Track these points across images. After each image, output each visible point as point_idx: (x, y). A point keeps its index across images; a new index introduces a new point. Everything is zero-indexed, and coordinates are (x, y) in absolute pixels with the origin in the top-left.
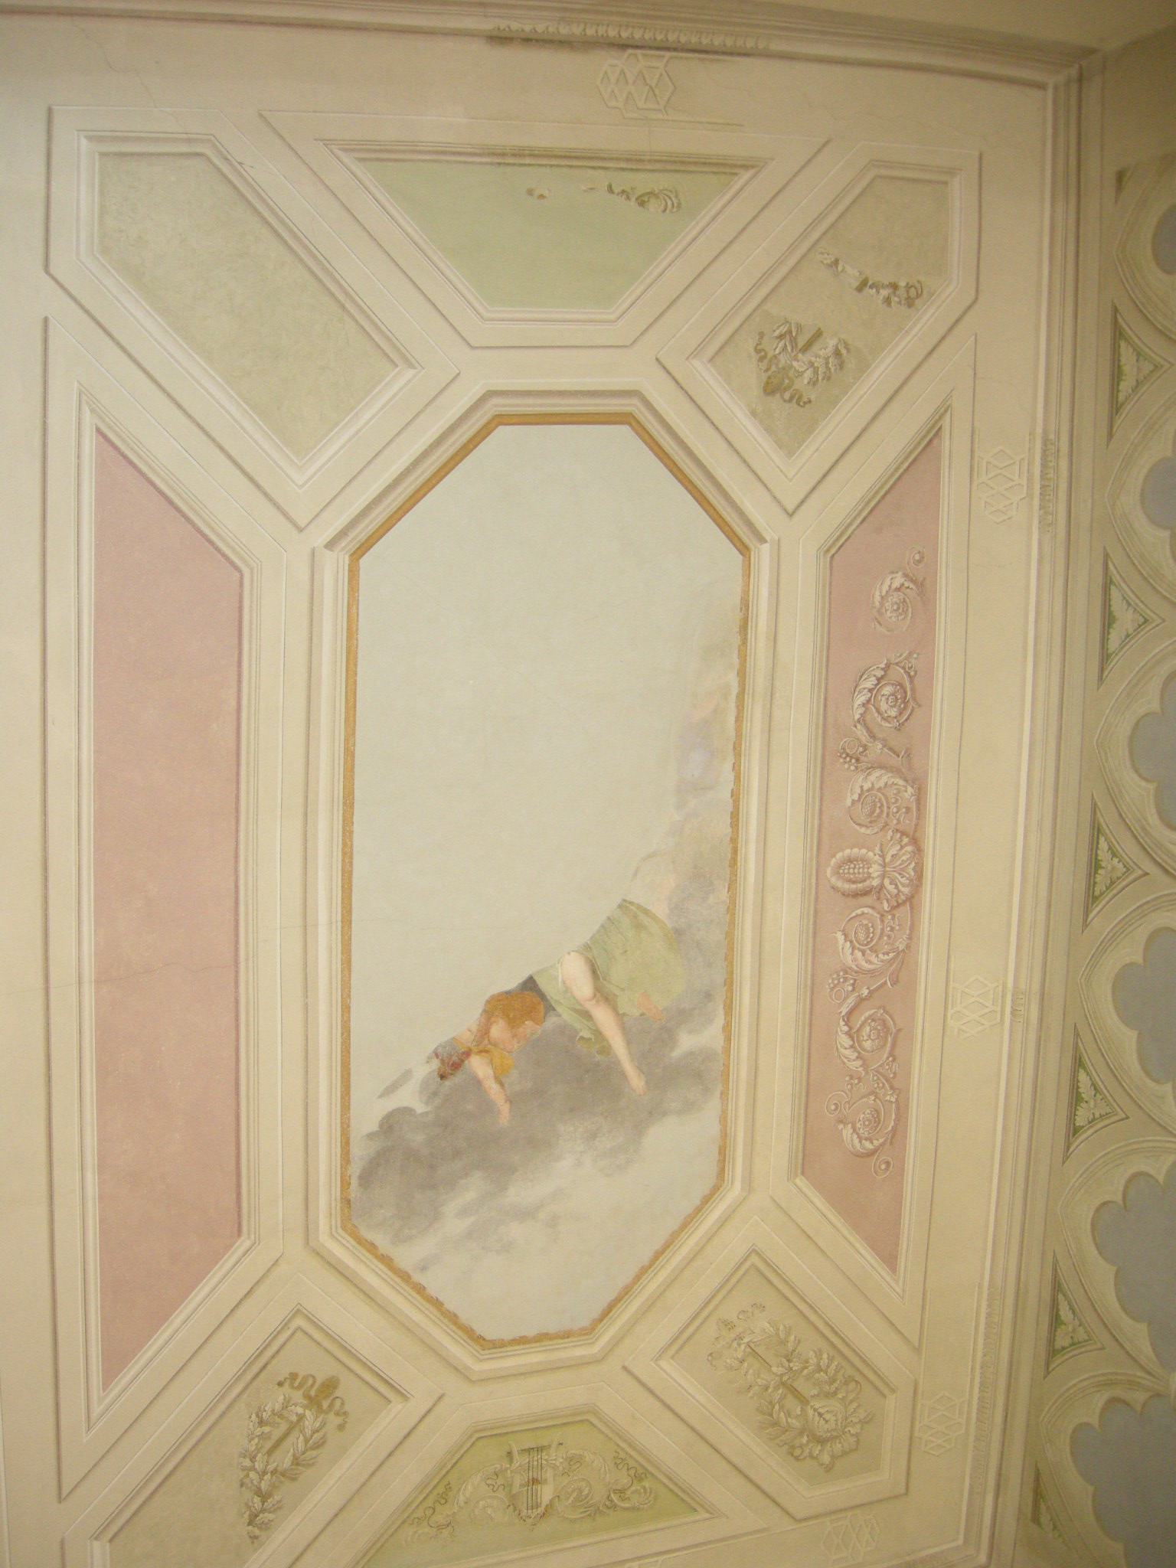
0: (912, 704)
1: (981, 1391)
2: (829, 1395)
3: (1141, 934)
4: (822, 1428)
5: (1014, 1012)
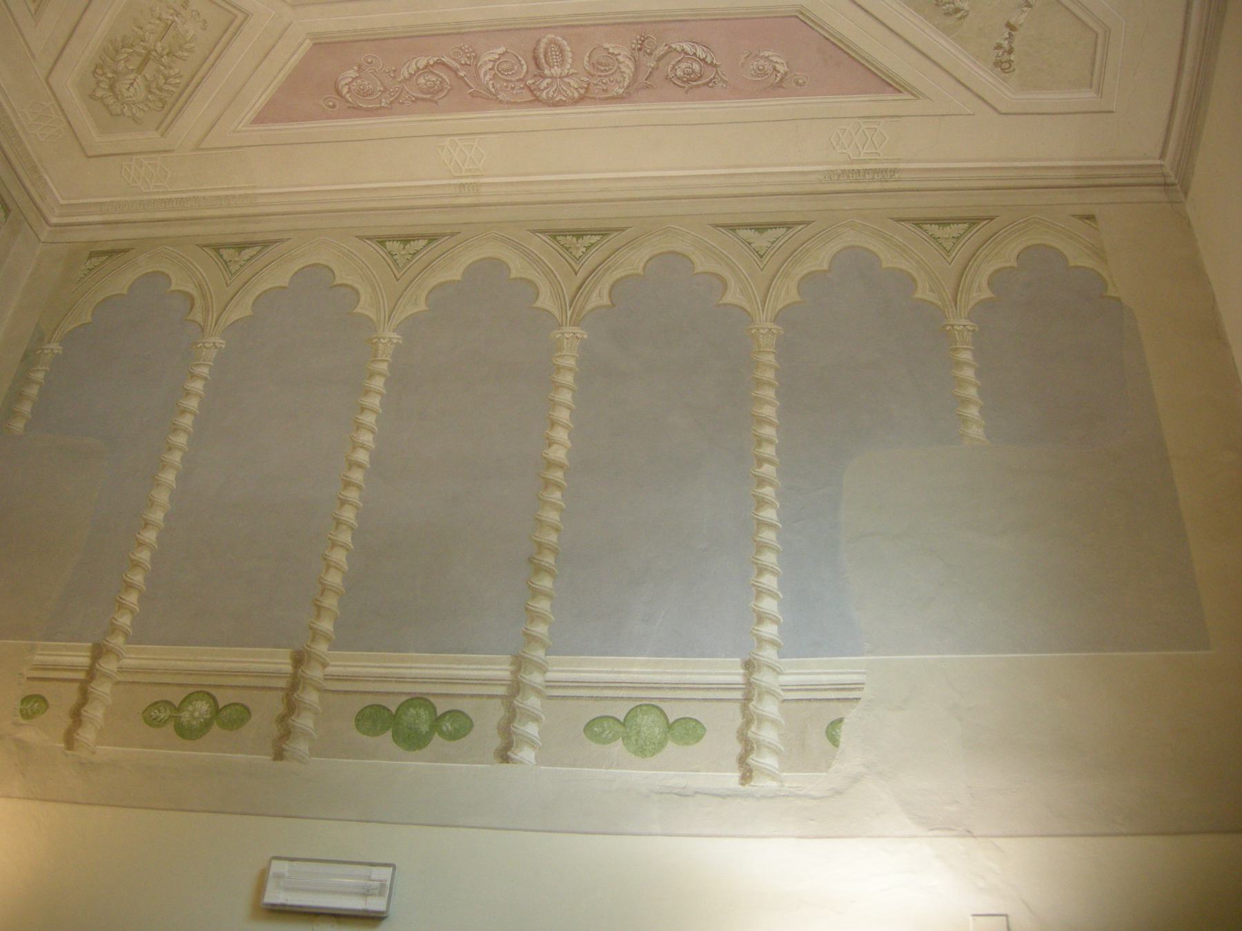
0: (687, 86)
1: (177, 199)
3: (532, 274)
5: (462, 185)
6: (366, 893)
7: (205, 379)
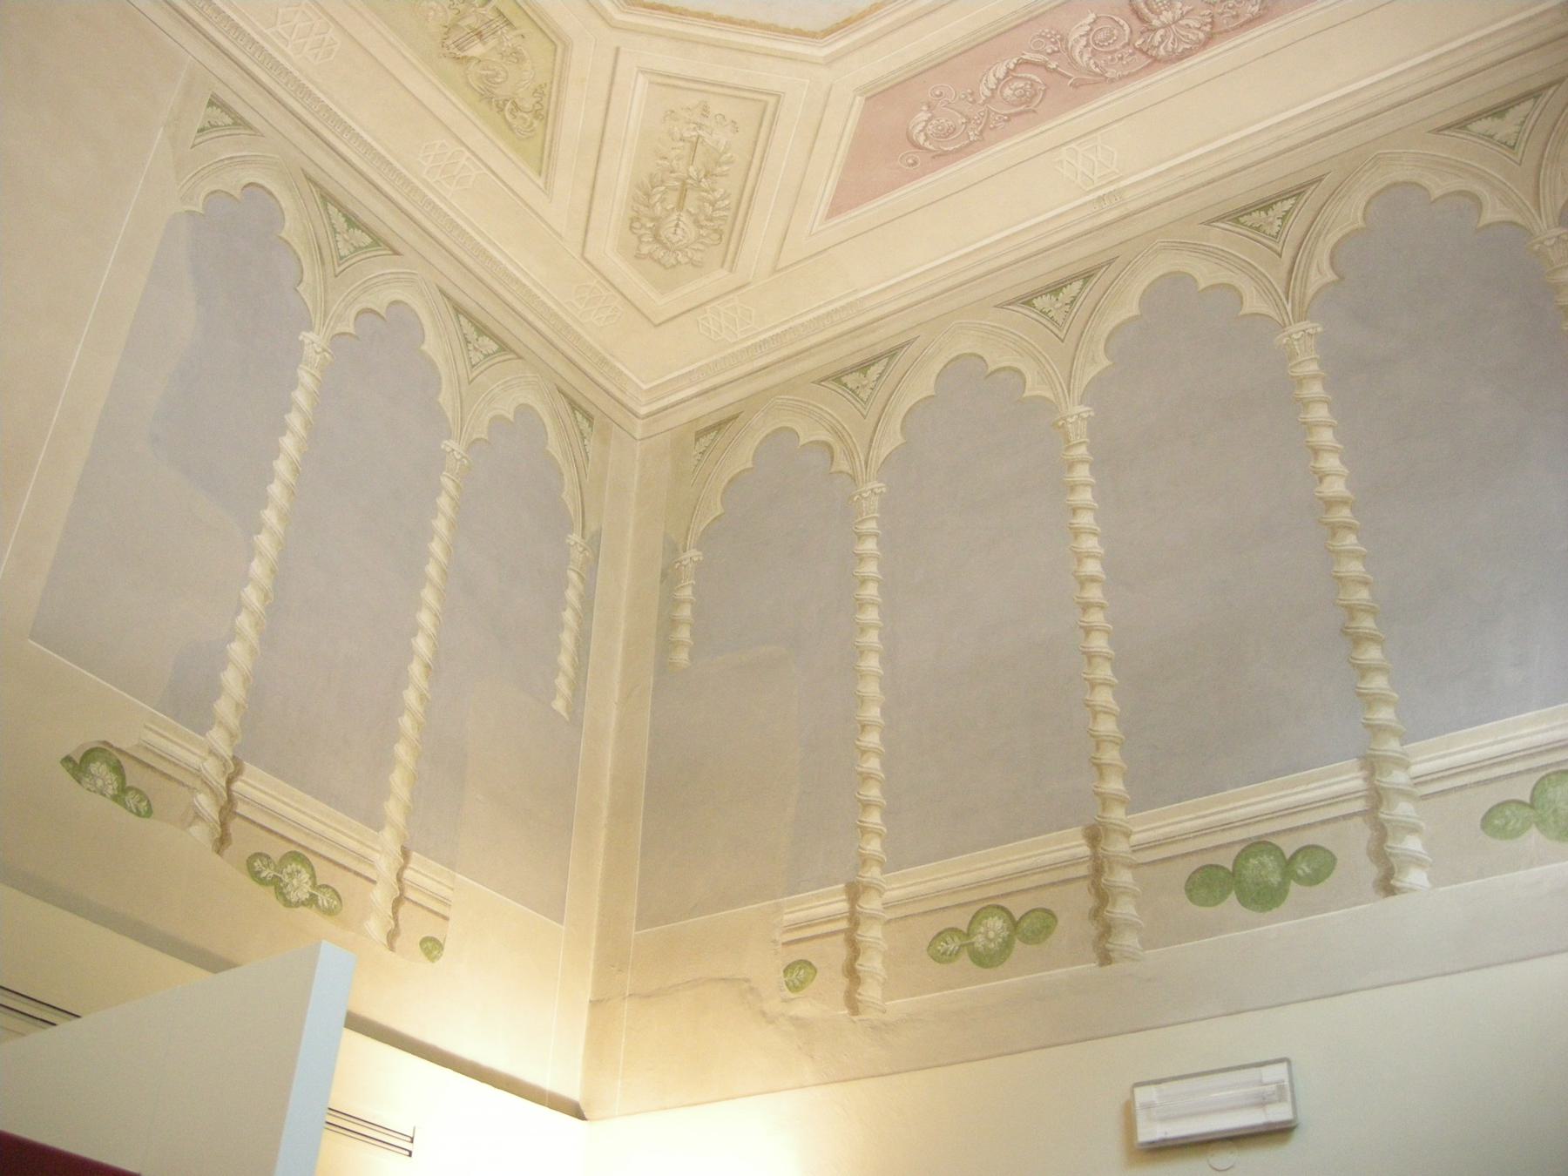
2: (697, 222)
3: (1224, 276)
4: (667, 231)
5: (1101, 199)
6: (1262, 1102)
7: (876, 535)
